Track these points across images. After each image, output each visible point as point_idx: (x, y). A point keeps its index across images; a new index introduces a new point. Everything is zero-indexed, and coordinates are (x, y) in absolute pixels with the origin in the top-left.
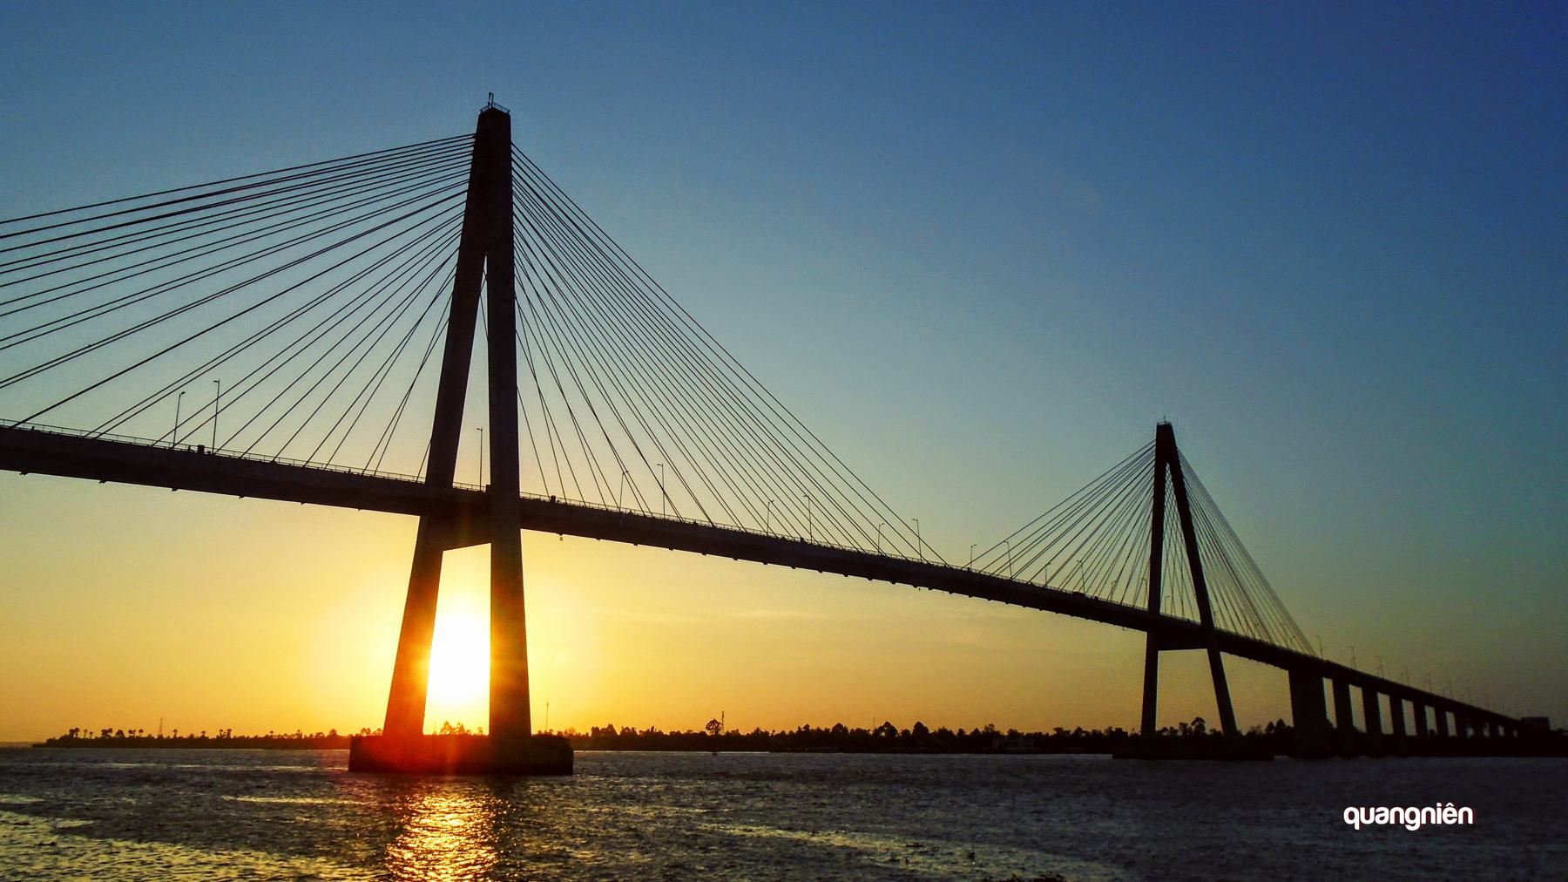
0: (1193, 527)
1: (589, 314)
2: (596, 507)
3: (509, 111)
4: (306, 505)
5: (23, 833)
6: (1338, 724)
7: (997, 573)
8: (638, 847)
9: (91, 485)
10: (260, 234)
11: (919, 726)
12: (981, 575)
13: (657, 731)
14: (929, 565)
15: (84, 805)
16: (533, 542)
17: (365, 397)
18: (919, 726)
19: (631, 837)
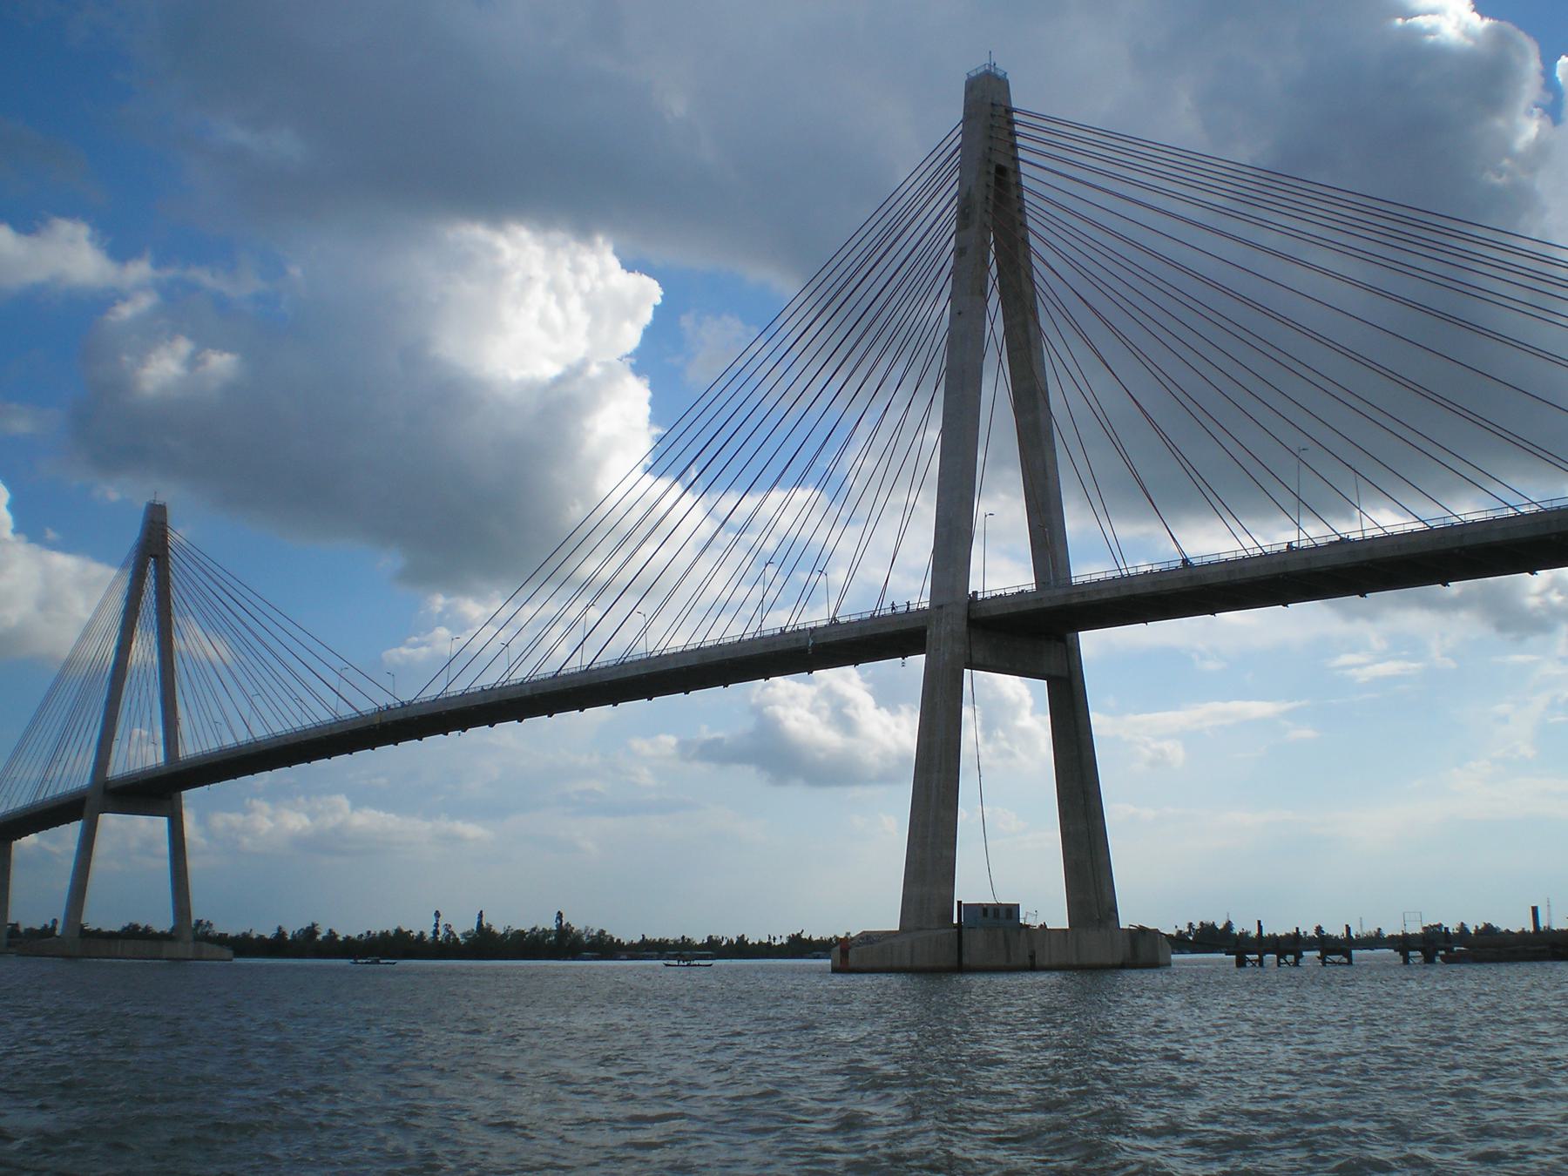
0: (156, 593)
1: (897, 330)
2: (1230, 556)
3: (1006, 73)
4: (657, 700)
5: (567, 1130)
6: (63, 931)
7: (792, 623)
8: (654, 1164)
9: (343, 759)
10: (1424, 225)
11: (741, 939)
12: (687, 652)
13: (1483, 925)
14: (1392, 536)
15: (1384, 1086)
16: (1092, 643)
17: (1183, 461)
18: (741, 939)
19: (1325, 1147)
